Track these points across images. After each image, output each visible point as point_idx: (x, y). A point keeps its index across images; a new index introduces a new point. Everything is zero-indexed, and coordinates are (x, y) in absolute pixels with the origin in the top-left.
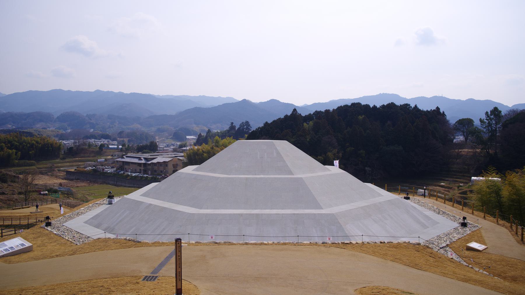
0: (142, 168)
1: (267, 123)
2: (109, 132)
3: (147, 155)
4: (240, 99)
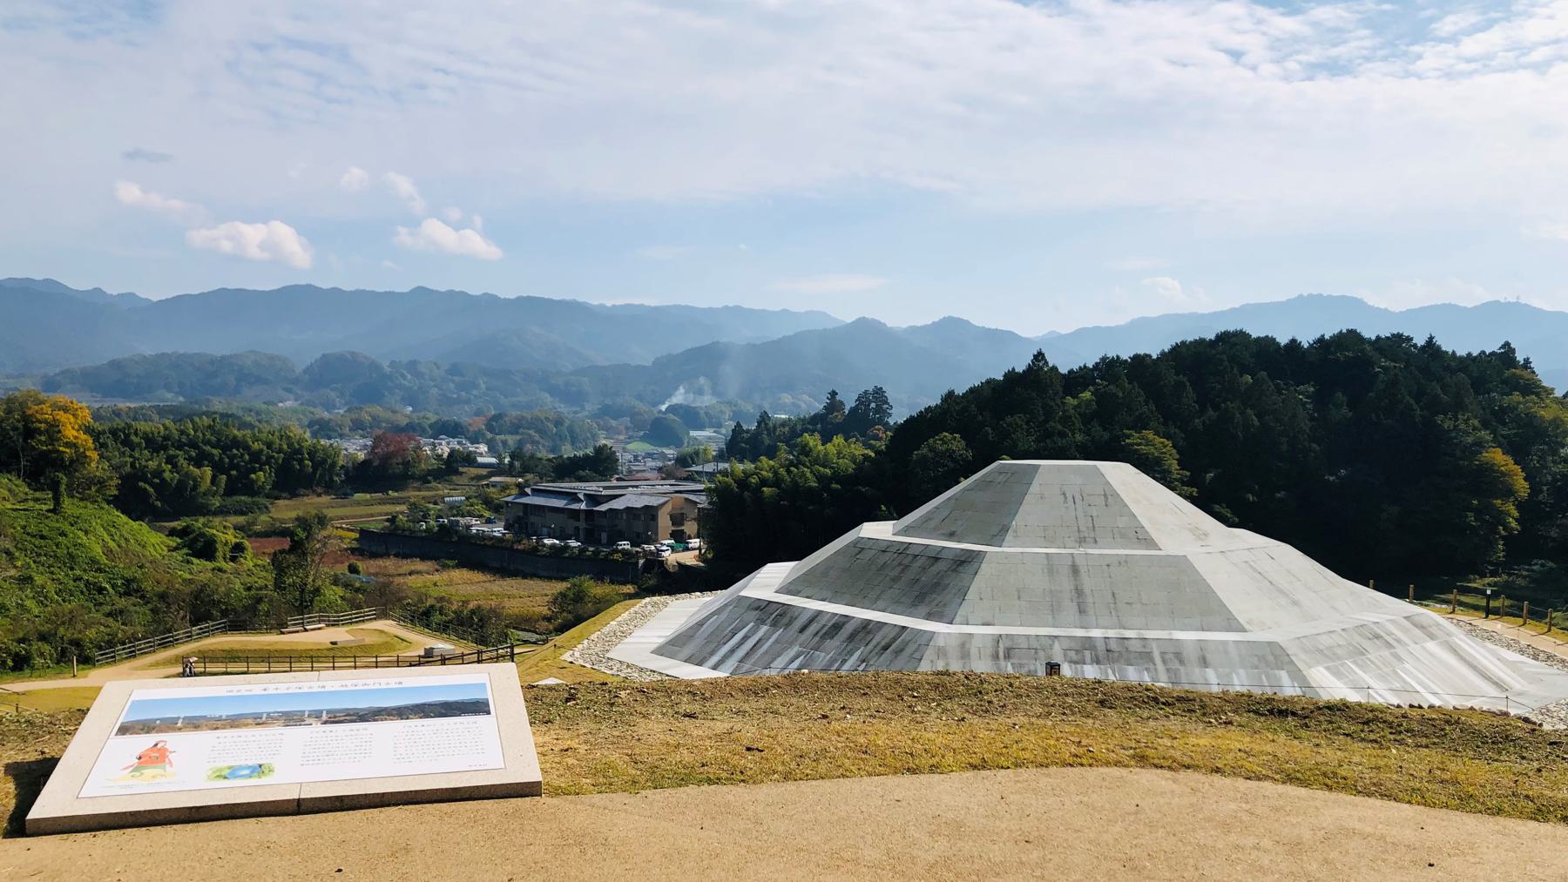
0: (582, 525)
2: (462, 415)
3: (593, 487)
4: (848, 317)
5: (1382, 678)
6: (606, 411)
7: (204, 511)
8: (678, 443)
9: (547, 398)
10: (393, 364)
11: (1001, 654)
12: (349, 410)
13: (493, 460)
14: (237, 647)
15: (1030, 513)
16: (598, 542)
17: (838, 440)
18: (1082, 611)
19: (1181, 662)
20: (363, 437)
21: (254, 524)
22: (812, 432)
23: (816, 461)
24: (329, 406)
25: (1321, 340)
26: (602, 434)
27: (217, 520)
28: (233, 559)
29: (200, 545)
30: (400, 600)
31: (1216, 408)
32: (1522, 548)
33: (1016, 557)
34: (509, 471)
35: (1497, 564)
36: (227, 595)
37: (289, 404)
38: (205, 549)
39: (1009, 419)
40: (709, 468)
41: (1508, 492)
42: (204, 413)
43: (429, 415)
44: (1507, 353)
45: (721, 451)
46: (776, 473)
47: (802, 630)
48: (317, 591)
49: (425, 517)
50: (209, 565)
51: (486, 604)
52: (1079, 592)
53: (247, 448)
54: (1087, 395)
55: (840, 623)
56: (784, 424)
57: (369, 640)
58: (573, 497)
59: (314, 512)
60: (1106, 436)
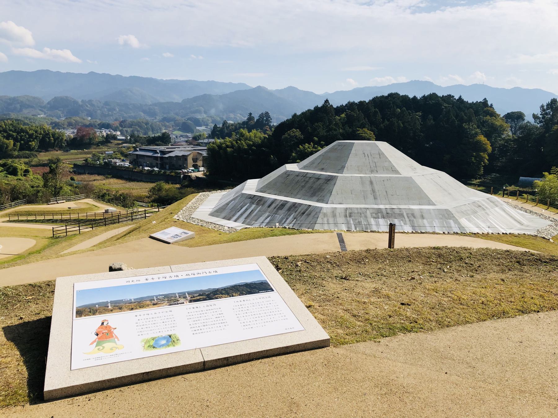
0: (159, 162)
1: (295, 115)
2: (110, 120)
3: (163, 148)
4: (254, 86)
5: (484, 222)
6: (165, 119)
7: (11, 157)
8: (191, 131)
9: (142, 114)
10: (82, 101)
11: (348, 215)
12: (66, 118)
13: (124, 138)
14: (31, 210)
15: (352, 161)
16: (165, 169)
17: (254, 131)
18: (375, 198)
19: (414, 217)
20: (72, 129)
21: (31, 162)
22: (244, 128)
23: (246, 139)
24: (59, 117)
25: (424, 96)
26: (163, 128)
27: (17, 160)
28: (25, 175)
29: (11, 170)
30: (92, 191)
31: (388, 120)
32: (489, 170)
33: (349, 177)
34: (130, 142)
35: (481, 175)
36: (25, 190)
37: (42, 116)
38: (13, 172)
39: (316, 124)
40: (206, 141)
41: (485, 150)
42: (9, 119)
43: (98, 121)
44: (485, 103)
45: (209, 135)
46: (232, 143)
47: (269, 206)
48: (61, 188)
49: (99, 159)
50: (16, 178)
51: (126, 192)
52: (373, 191)
53: (27, 133)
54: (343, 115)
55: (283, 204)
56: (232, 125)
57: (83, 207)
58: (155, 152)
59: (55, 157)
60: (351, 130)
